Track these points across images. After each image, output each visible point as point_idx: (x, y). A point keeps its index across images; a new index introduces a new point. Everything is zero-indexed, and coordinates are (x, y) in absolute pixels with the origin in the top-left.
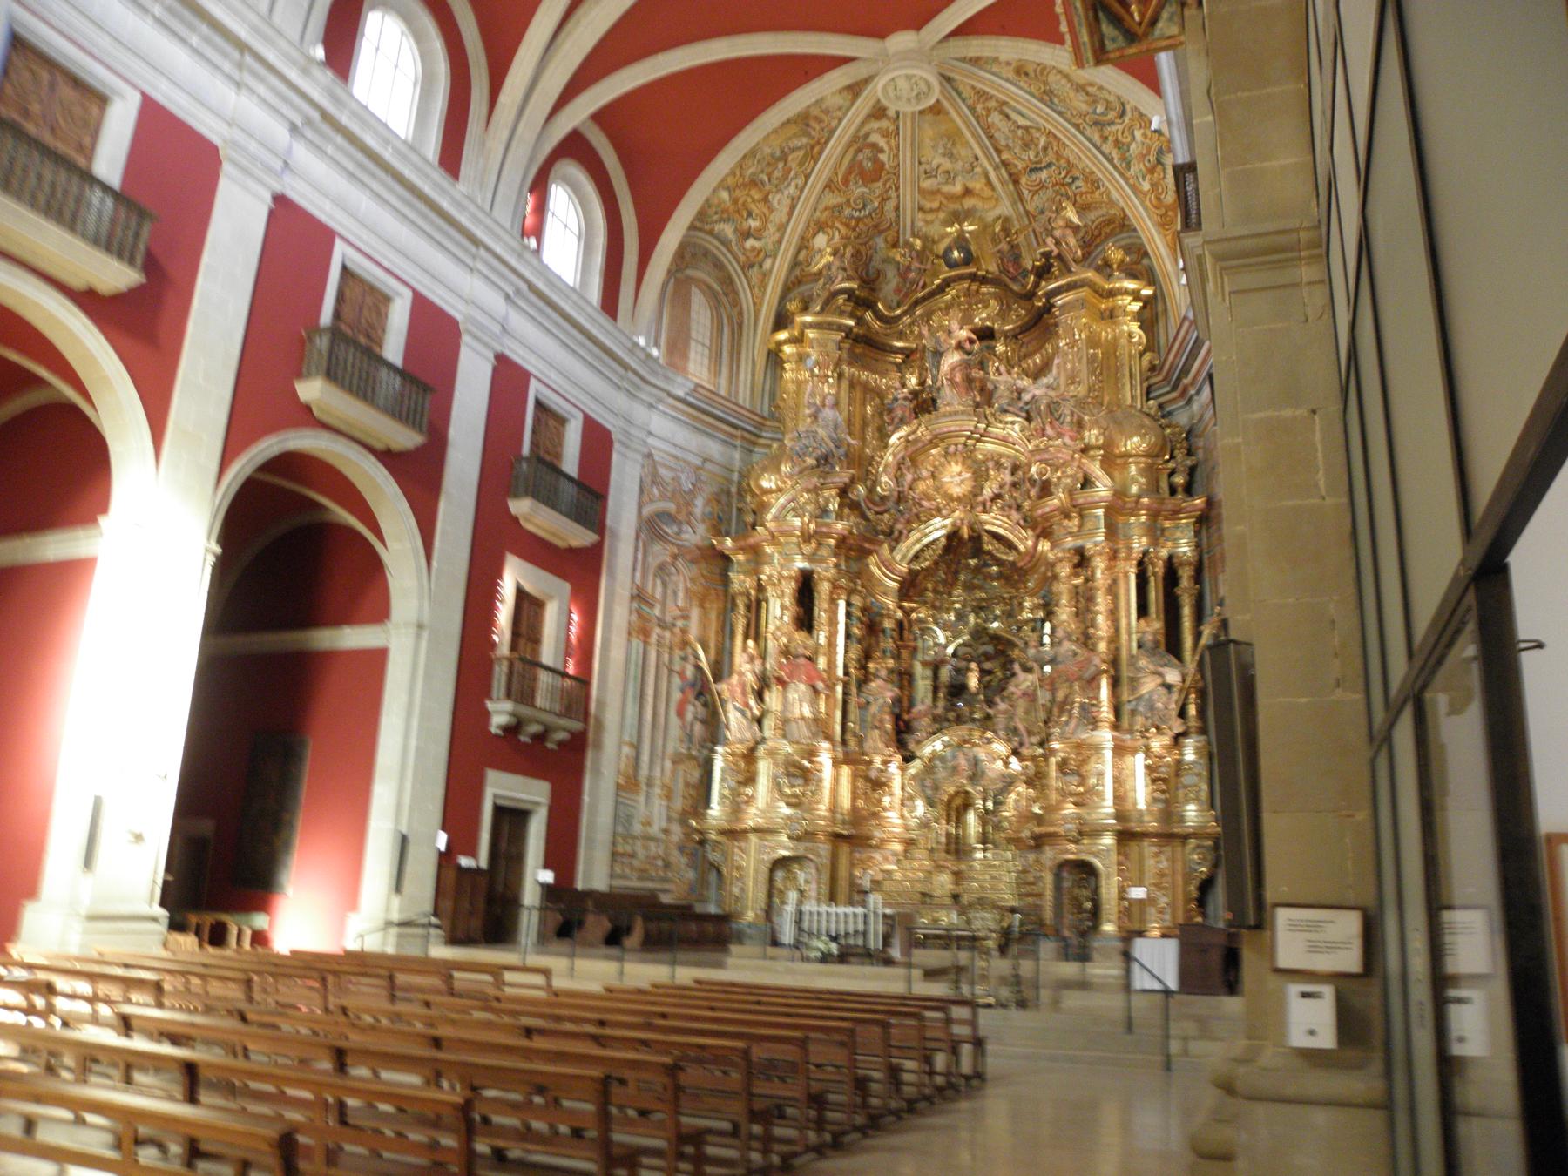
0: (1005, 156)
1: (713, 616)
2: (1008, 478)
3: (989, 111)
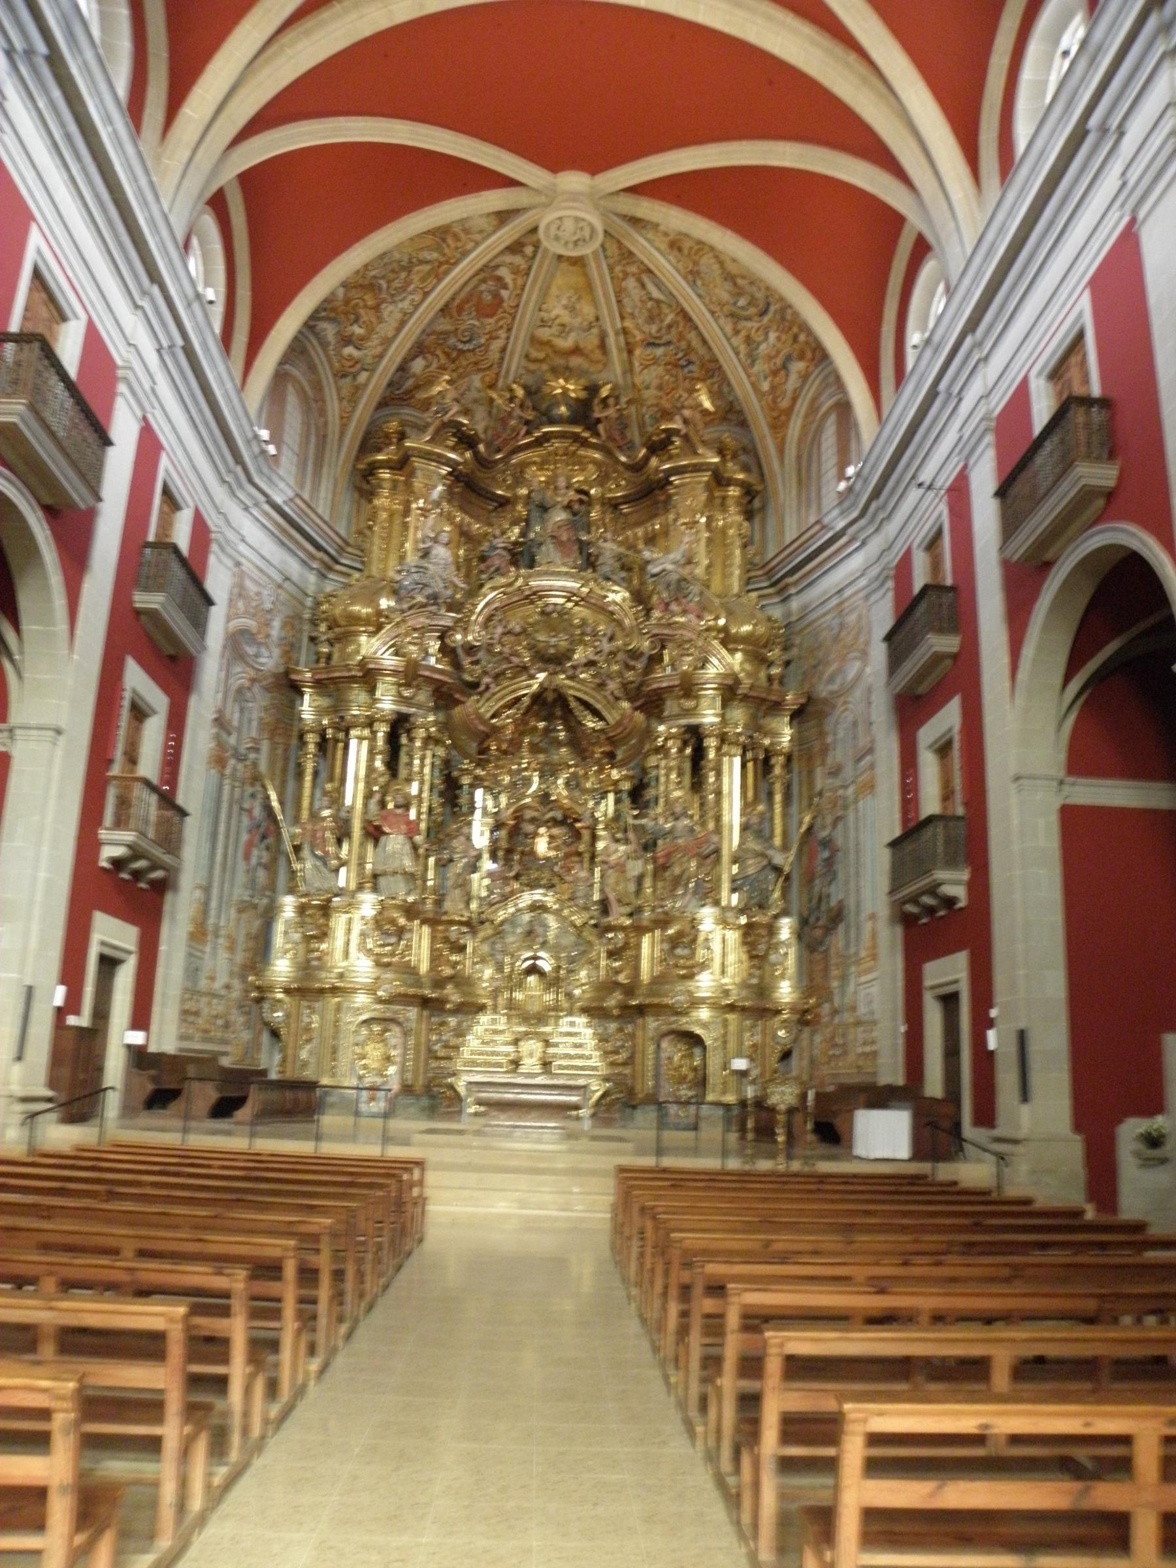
0: (628, 324)
3: (626, 275)
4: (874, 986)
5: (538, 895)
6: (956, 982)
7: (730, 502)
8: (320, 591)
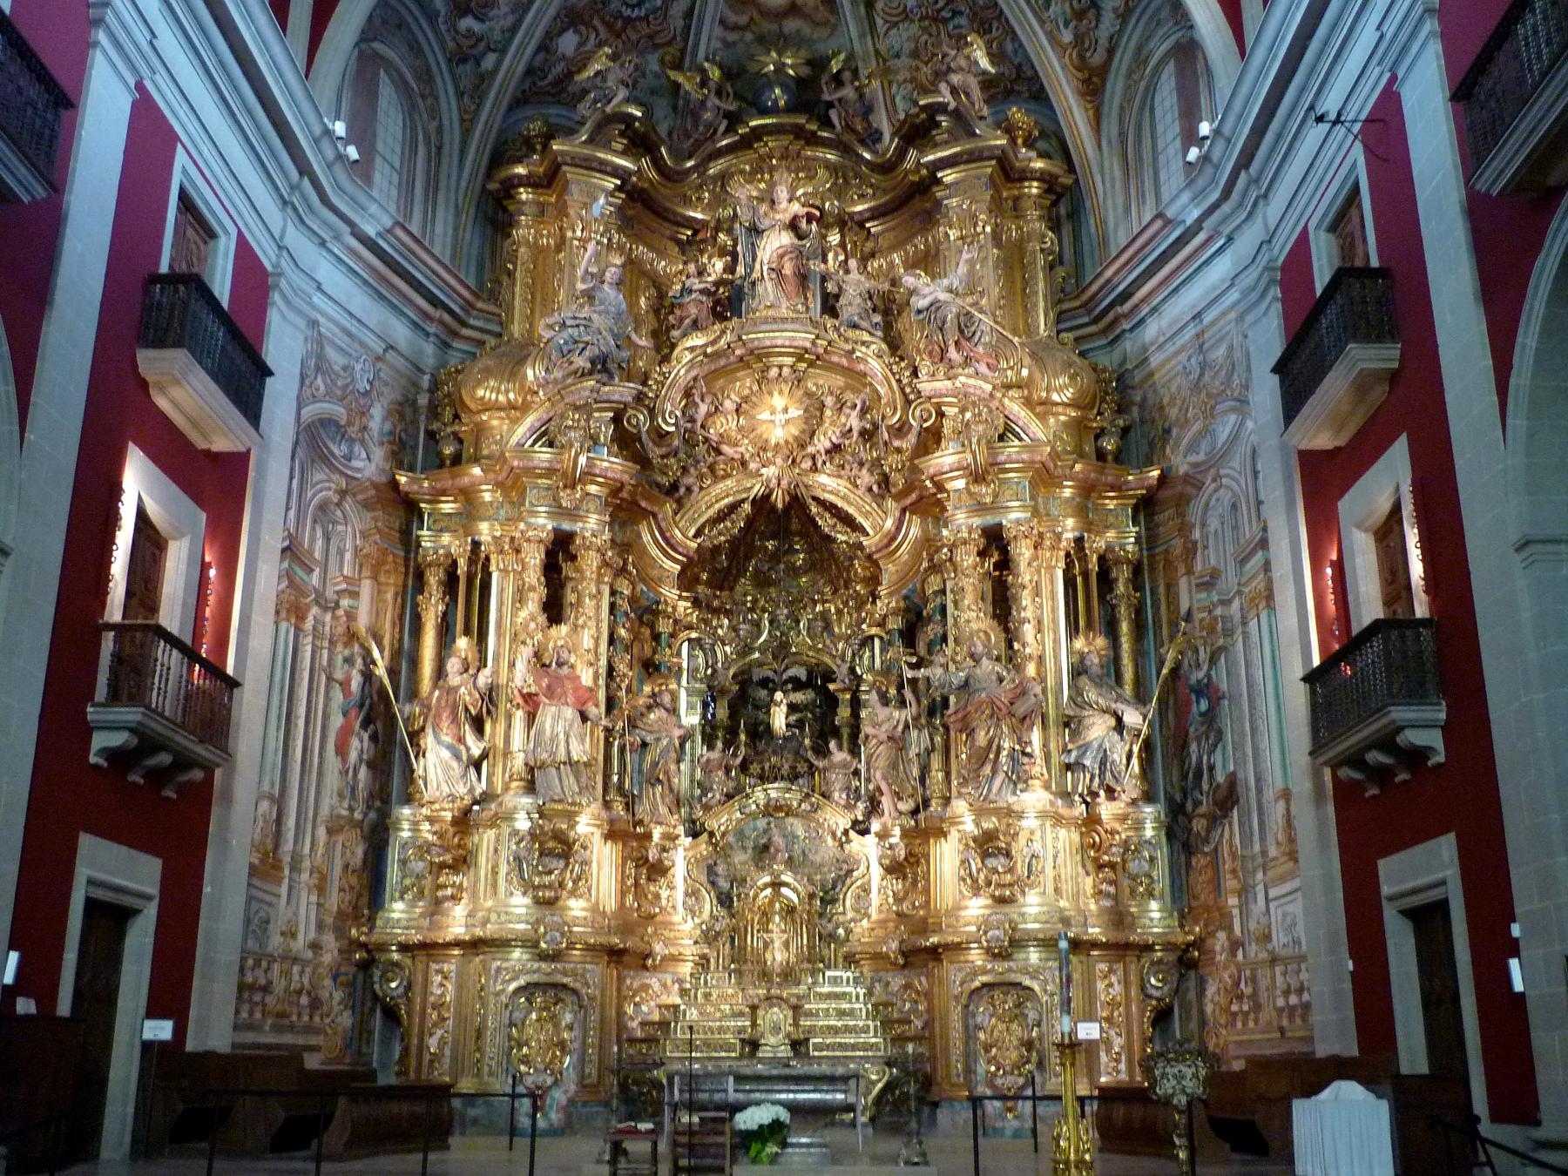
4: (1286, 906)
5: (775, 791)
6: (1443, 883)
7: (1026, 204)
8: (443, 364)
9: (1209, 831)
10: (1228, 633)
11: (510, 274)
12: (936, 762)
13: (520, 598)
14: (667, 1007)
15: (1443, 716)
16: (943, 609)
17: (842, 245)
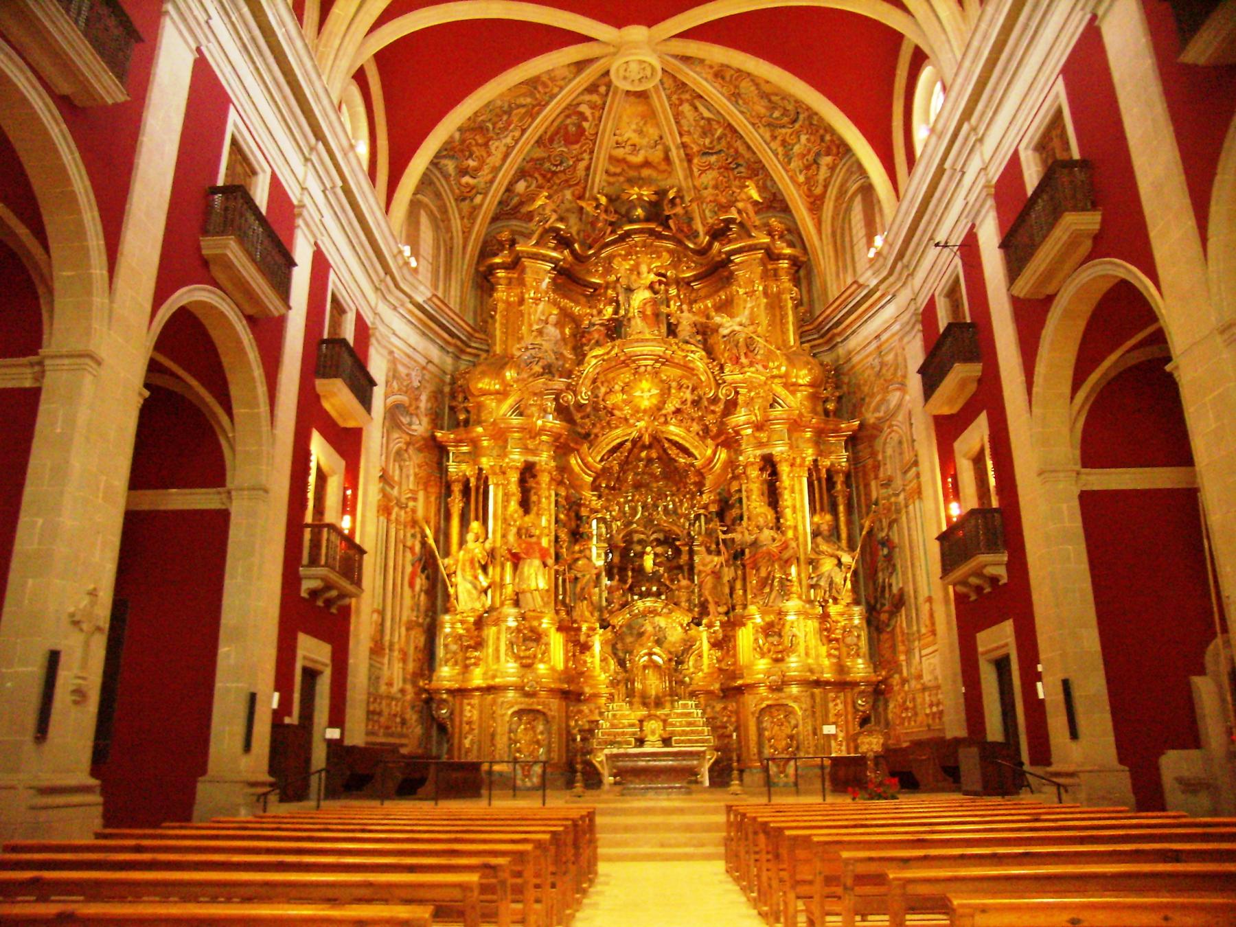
0: (686, 139)
1: (433, 499)
2: (688, 396)
3: (681, 102)
5: (649, 602)
7: (781, 273)
8: (457, 369)
9: (889, 620)
10: (898, 511)
11: (493, 317)
12: (738, 585)
13: (507, 497)
14: (592, 722)
15: (1006, 559)
16: (740, 500)
17: (678, 296)
